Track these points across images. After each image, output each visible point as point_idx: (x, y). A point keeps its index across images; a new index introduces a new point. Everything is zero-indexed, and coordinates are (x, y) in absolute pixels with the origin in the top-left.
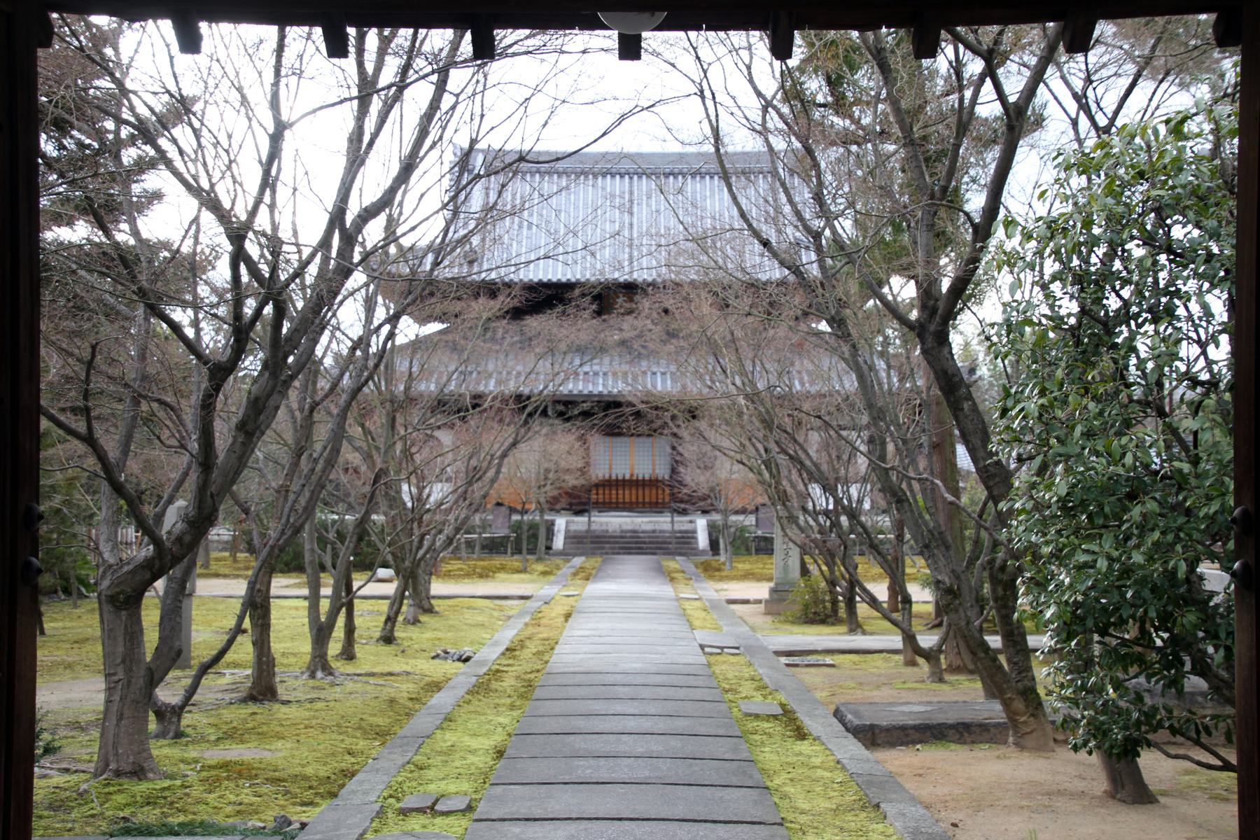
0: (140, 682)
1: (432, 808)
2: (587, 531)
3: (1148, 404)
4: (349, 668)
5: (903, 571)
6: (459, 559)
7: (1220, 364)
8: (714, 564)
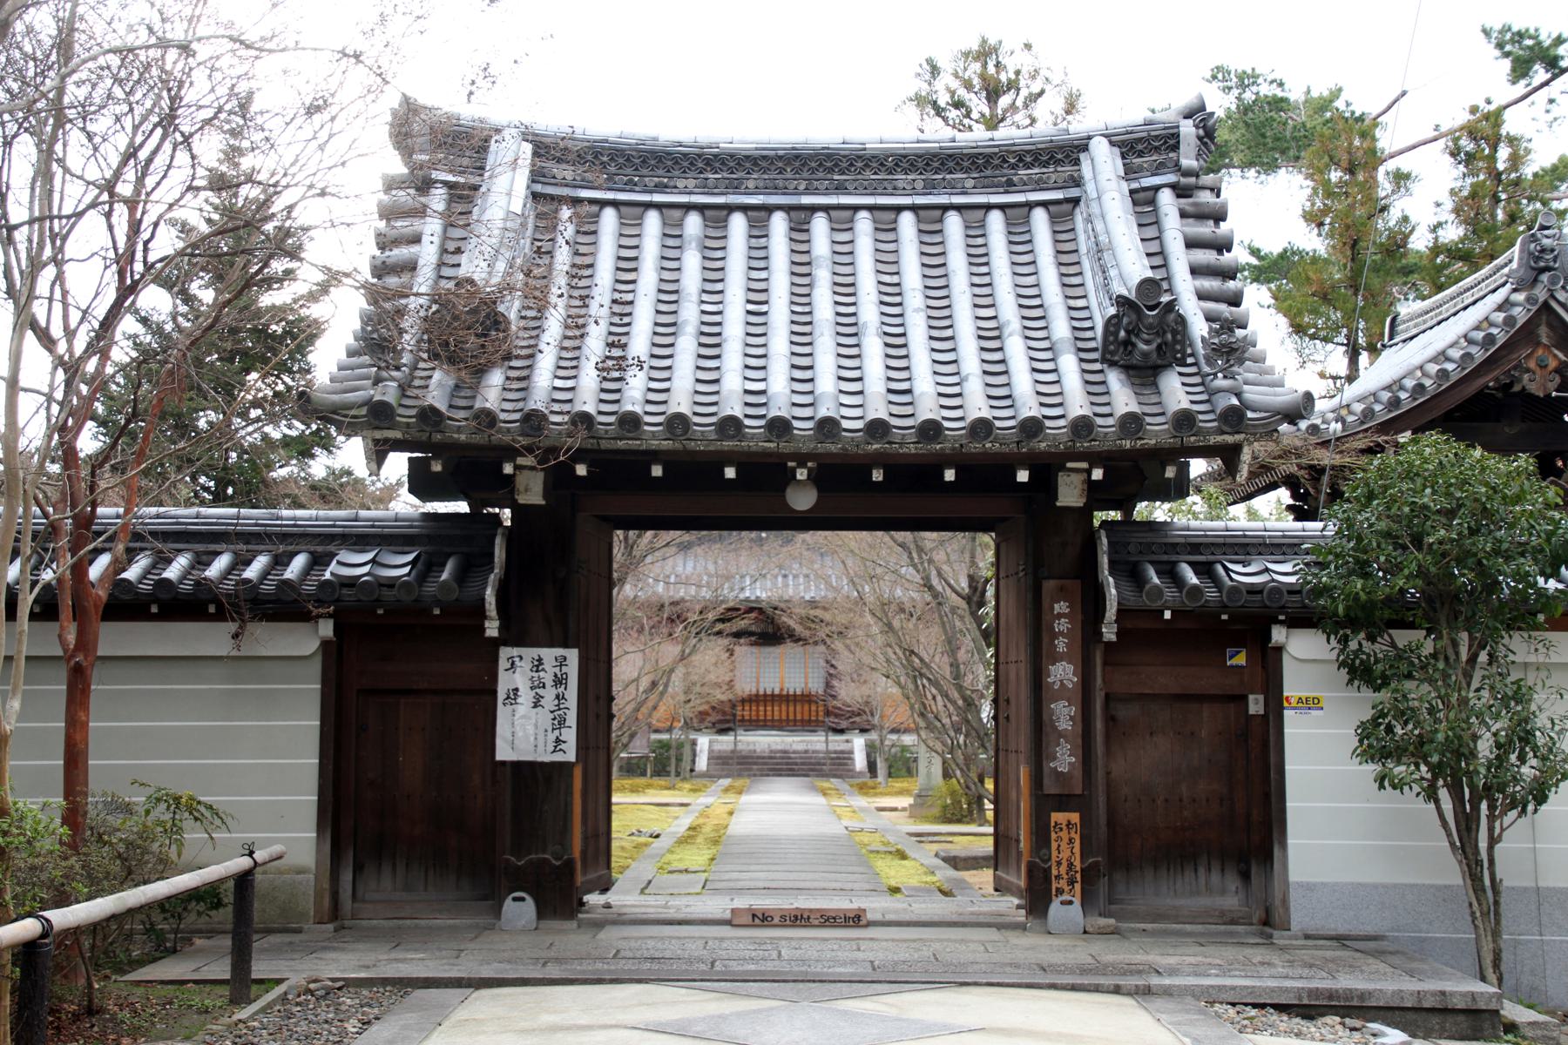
2: (733, 752)
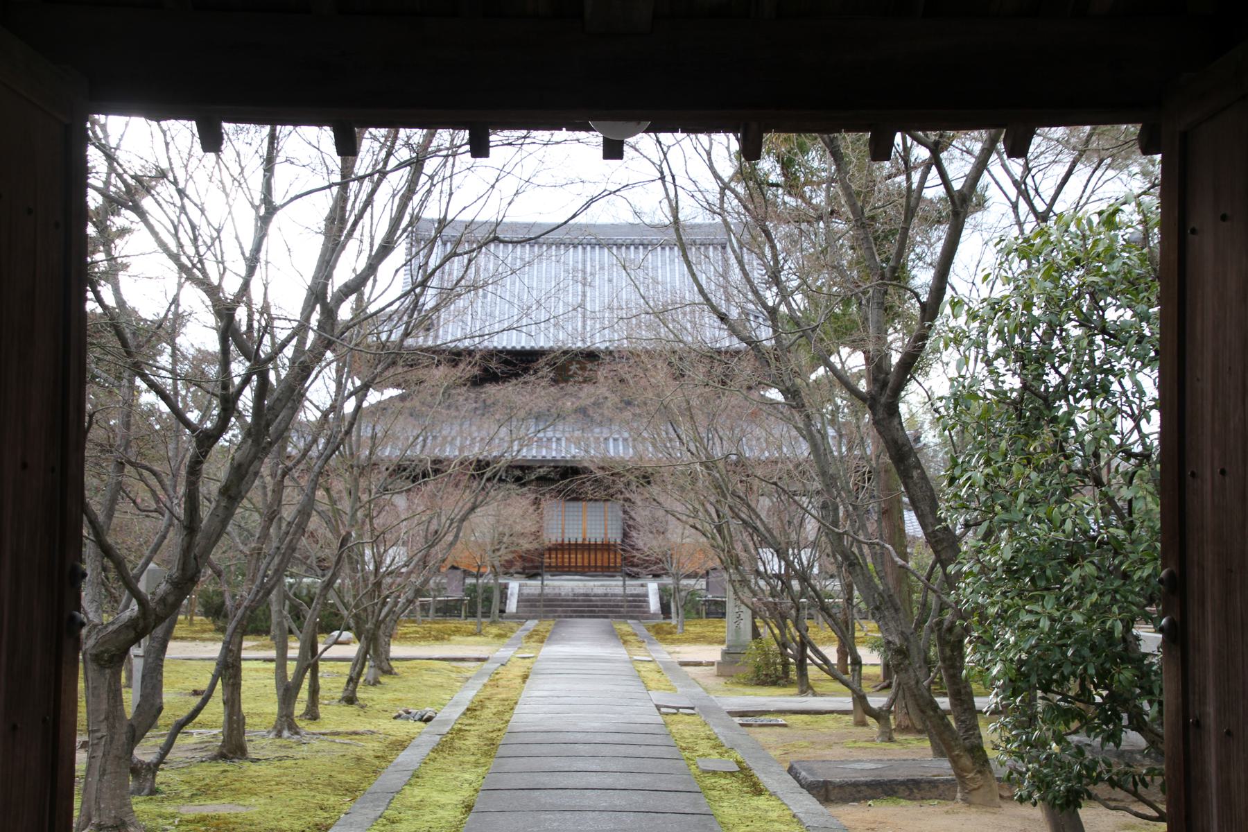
0: (122, 738)
2: (540, 595)
3: (1086, 474)
4: (314, 728)
5: (853, 634)
6: (414, 622)
7: (1152, 437)
8: (666, 627)
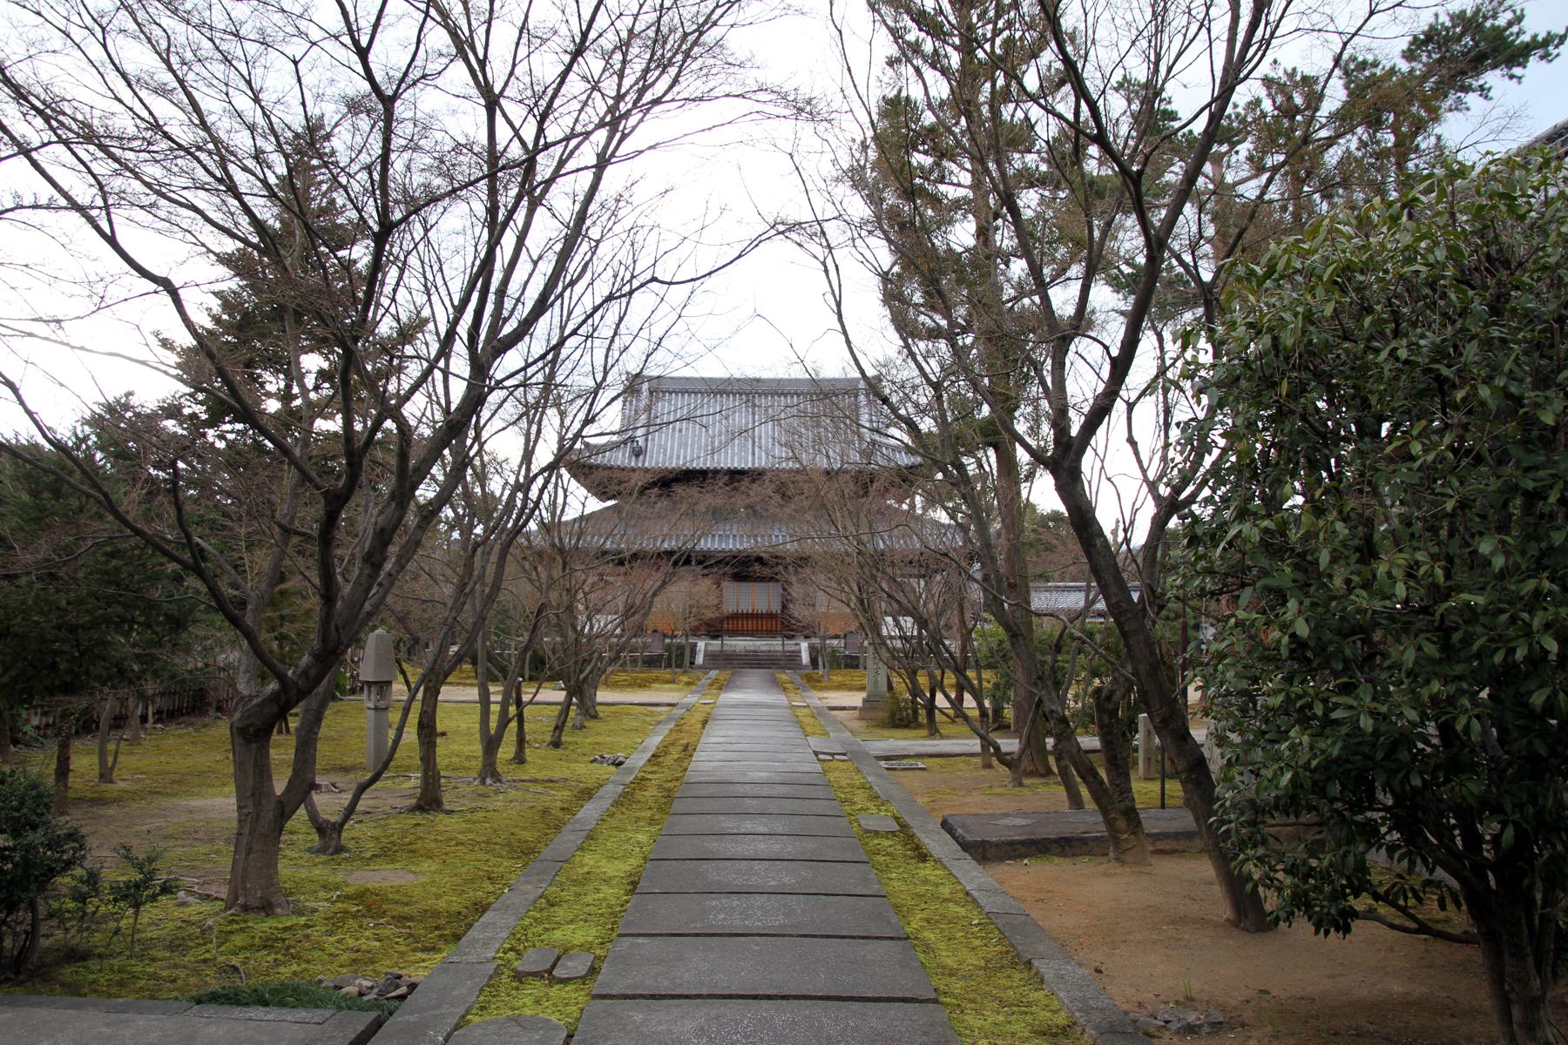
0: (269, 814)
1: (550, 972)
